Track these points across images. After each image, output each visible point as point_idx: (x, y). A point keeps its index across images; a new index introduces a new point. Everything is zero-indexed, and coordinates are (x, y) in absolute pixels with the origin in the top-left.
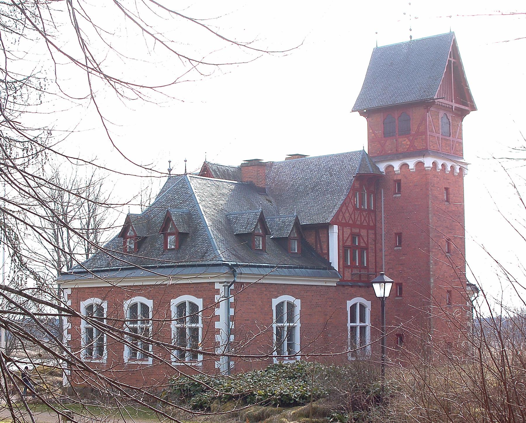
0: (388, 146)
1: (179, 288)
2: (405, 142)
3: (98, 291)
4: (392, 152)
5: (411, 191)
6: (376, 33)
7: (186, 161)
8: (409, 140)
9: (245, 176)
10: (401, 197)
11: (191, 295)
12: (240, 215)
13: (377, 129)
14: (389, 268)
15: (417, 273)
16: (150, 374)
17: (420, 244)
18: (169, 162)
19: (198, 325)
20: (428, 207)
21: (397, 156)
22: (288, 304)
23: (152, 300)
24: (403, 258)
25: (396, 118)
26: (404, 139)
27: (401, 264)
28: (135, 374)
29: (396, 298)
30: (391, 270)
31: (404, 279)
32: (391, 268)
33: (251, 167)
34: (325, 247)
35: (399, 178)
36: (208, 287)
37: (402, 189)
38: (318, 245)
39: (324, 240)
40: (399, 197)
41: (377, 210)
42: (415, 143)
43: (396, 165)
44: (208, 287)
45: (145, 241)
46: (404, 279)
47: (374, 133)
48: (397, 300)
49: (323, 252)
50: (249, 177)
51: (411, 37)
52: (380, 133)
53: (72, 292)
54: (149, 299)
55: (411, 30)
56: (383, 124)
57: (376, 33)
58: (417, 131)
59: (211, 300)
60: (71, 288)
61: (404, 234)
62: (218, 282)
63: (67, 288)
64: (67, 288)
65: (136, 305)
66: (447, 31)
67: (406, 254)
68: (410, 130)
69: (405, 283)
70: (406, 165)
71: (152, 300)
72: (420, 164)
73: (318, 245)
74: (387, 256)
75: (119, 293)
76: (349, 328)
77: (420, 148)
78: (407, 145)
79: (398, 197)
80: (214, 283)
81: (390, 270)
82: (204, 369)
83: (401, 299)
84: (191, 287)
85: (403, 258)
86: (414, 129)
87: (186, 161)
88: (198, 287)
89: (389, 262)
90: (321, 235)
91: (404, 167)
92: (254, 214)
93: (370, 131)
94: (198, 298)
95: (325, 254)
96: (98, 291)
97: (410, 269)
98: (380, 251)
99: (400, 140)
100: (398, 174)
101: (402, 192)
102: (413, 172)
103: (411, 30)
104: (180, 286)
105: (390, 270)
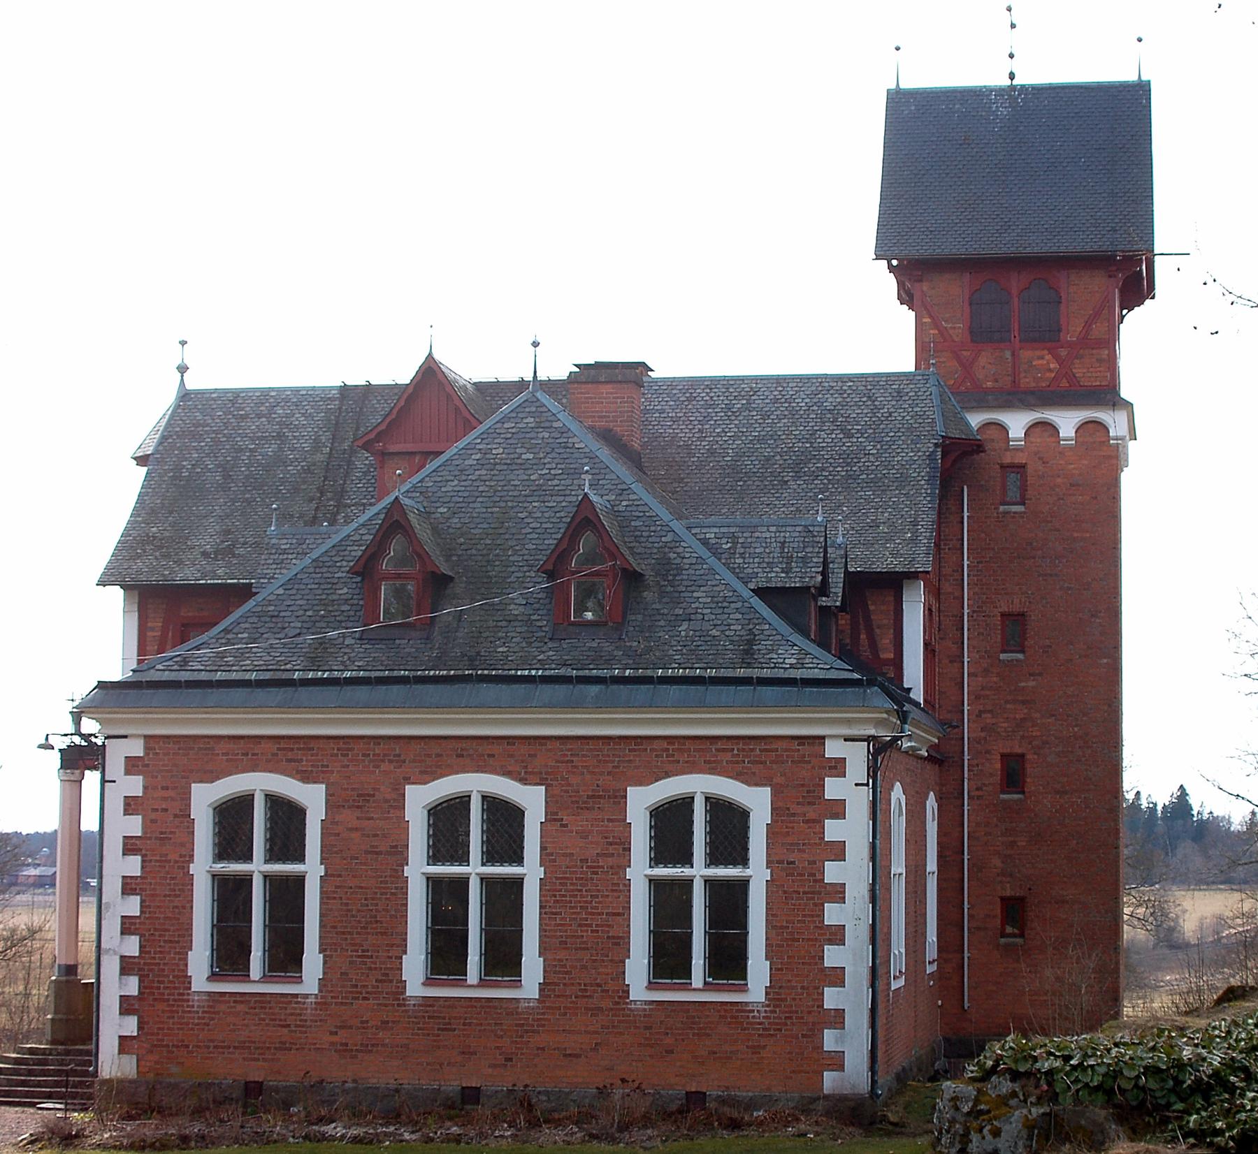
0: (984, 367)
1: (667, 750)
2: (1040, 362)
3: (279, 749)
4: (997, 385)
5: (1059, 499)
6: (1140, 40)
7: (535, 344)
8: (1057, 358)
9: (584, 412)
10: (1025, 513)
11: (719, 774)
12: (744, 529)
13: (947, 315)
14: (980, 711)
15: (1076, 729)
16: (527, 1031)
17: (1085, 647)
18: (180, 342)
19: (748, 872)
20: (1115, 548)
21: (1016, 398)
22: (272, 801)
23: (544, 787)
24: (1032, 684)
25: (1015, 292)
26: (1038, 353)
27: (1023, 702)
28: (455, 1030)
29: (1002, 796)
30: (989, 715)
31: (1030, 743)
32: (989, 711)
33: (609, 386)
34: (886, 641)
35: (1020, 459)
36: (793, 751)
37: (1030, 493)
38: (863, 636)
39: (885, 622)
40: (1021, 513)
41: (945, 545)
42: (1075, 368)
43: (1017, 424)
44: (793, 751)
45: (448, 591)
46: (1030, 743)
47: (936, 324)
48: (1004, 801)
49: (881, 656)
50: (599, 417)
51: (1012, 76)
52: (958, 329)
53: (147, 749)
54: (524, 781)
55: (1011, 56)
56: (970, 304)
57: (1140, 40)
58: (1082, 335)
59: (808, 792)
60: (146, 737)
61: (1033, 618)
62: (841, 736)
63: (125, 737)
64: (125, 737)
65: (460, 804)
66: (1131, 77)
67: (1040, 674)
68: (1060, 331)
69: (1035, 754)
70: (1049, 428)
71: (544, 787)
72: (1090, 425)
73: (863, 636)
74: (976, 676)
75: (383, 761)
76: (58, 864)
77: (1090, 384)
78: (1050, 370)
79: (1015, 513)
80: (823, 738)
81: (983, 716)
82: (771, 1012)
83: (1020, 800)
84: (717, 750)
85: (1032, 684)
86: (1072, 331)
87: (535, 344)
88: (752, 750)
89: (982, 693)
90: (872, 608)
91: (1038, 430)
92: (798, 529)
93: (924, 320)
94: (749, 785)
95: (887, 662)
96: (279, 749)
97: (1053, 715)
98: (950, 662)
99: (1025, 354)
100: (1017, 449)
101: (1030, 499)
102: (1070, 448)
103: (1011, 56)
104: (668, 743)
105: (983, 716)
